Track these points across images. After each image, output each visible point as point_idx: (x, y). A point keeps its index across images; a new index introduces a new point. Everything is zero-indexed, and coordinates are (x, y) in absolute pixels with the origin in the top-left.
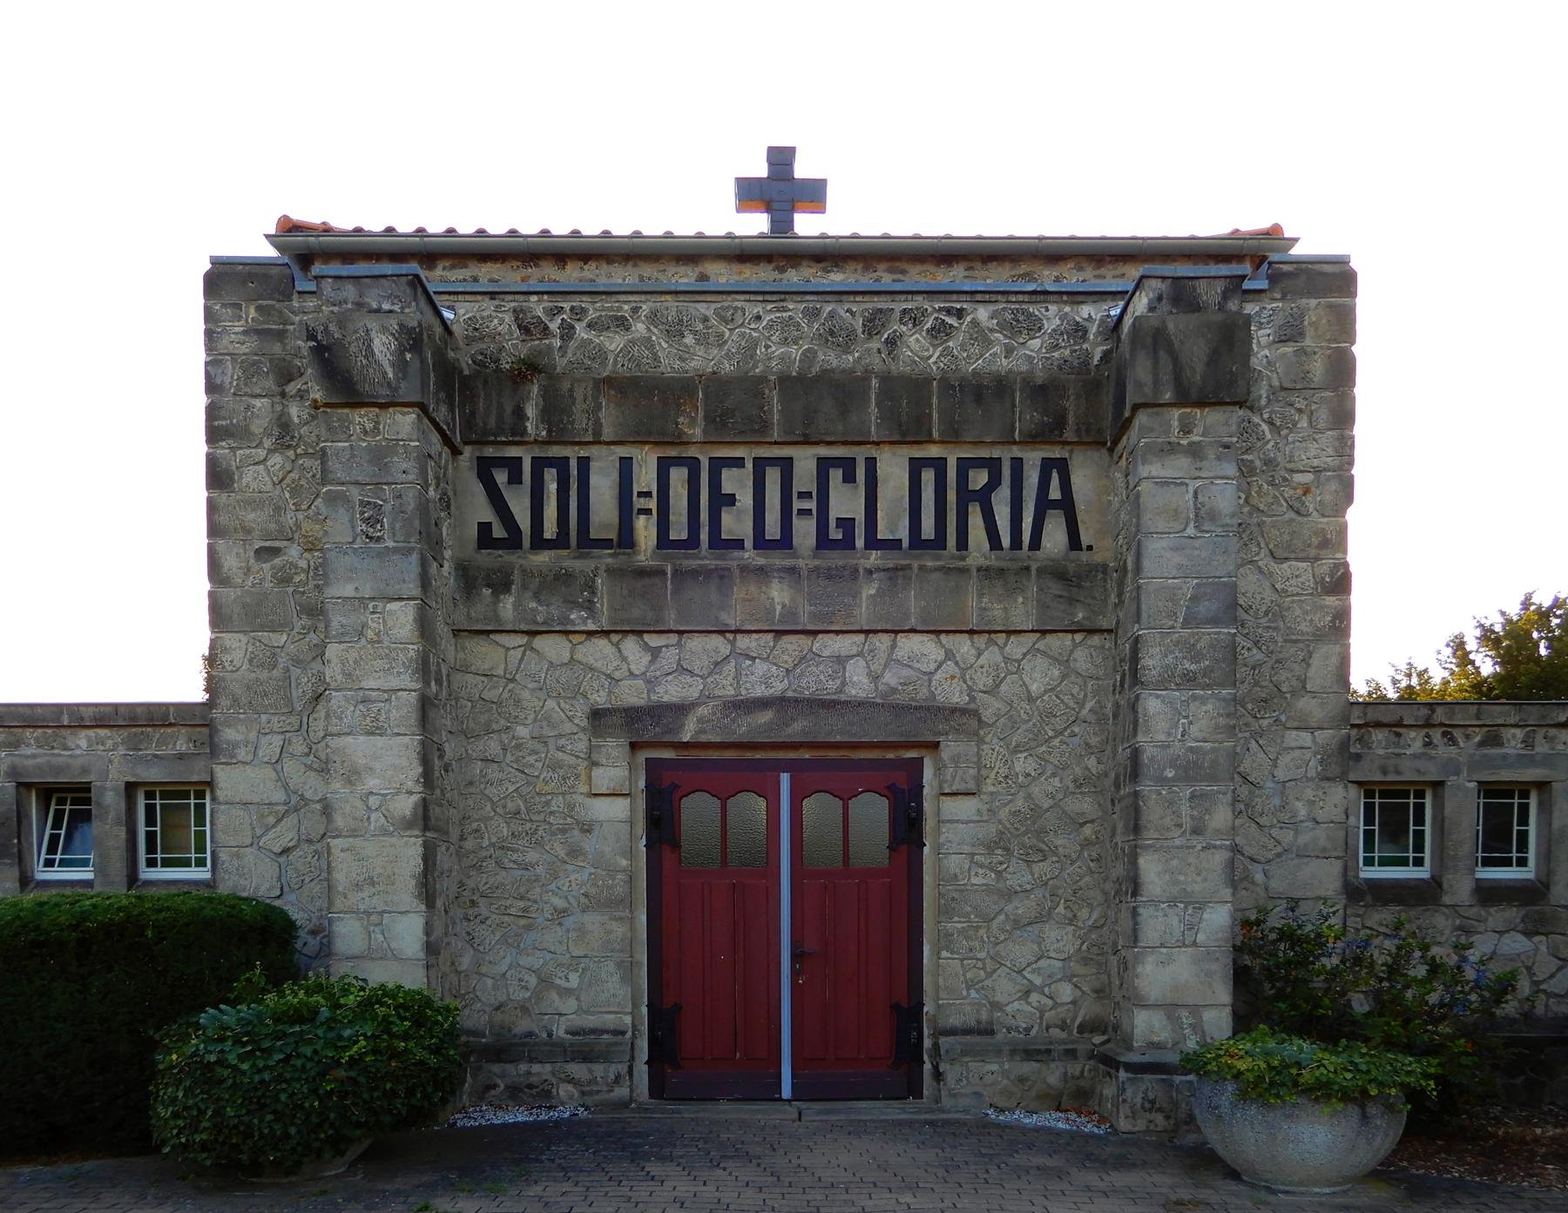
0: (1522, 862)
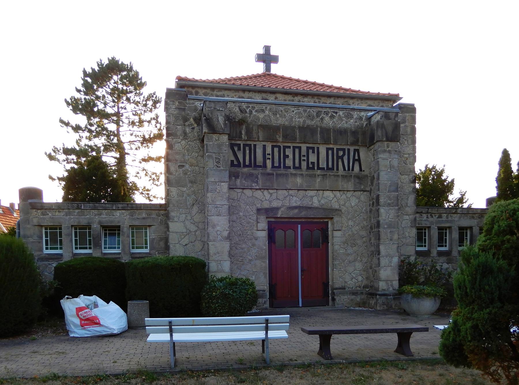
0: (446, 246)
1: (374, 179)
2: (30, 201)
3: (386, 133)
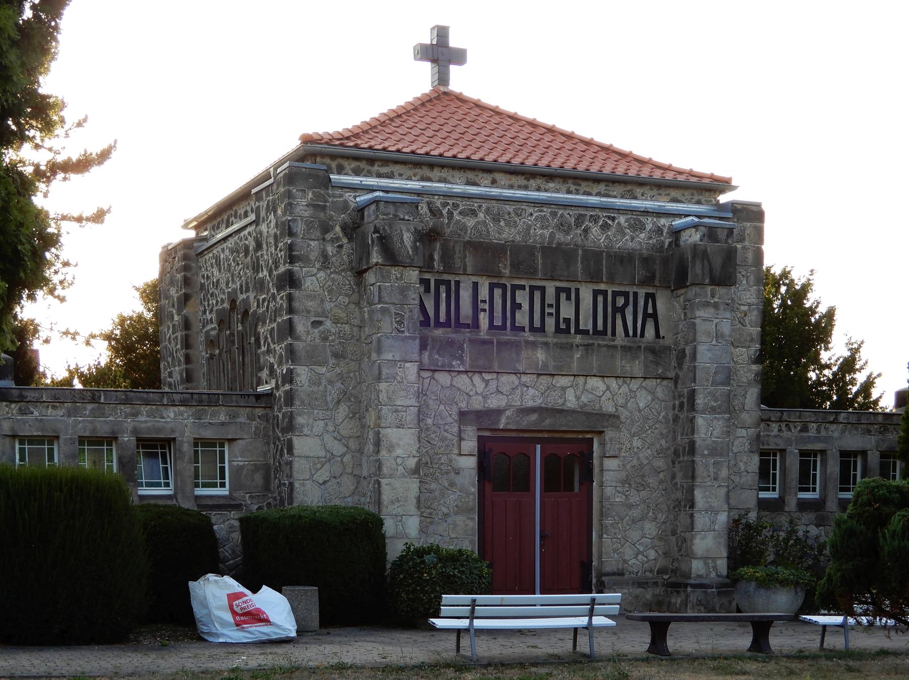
0: (814, 490)
1: (684, 357)
3: (711, 270)
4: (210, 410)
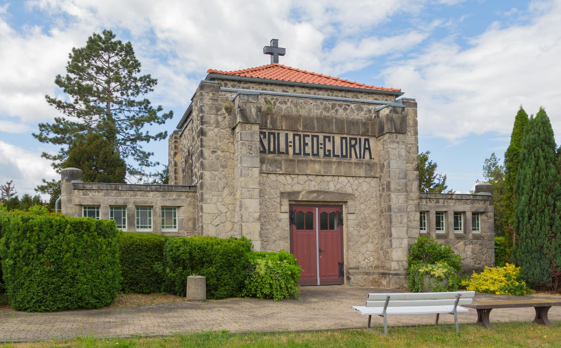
2: (73, 181)
4: (169, 193)
